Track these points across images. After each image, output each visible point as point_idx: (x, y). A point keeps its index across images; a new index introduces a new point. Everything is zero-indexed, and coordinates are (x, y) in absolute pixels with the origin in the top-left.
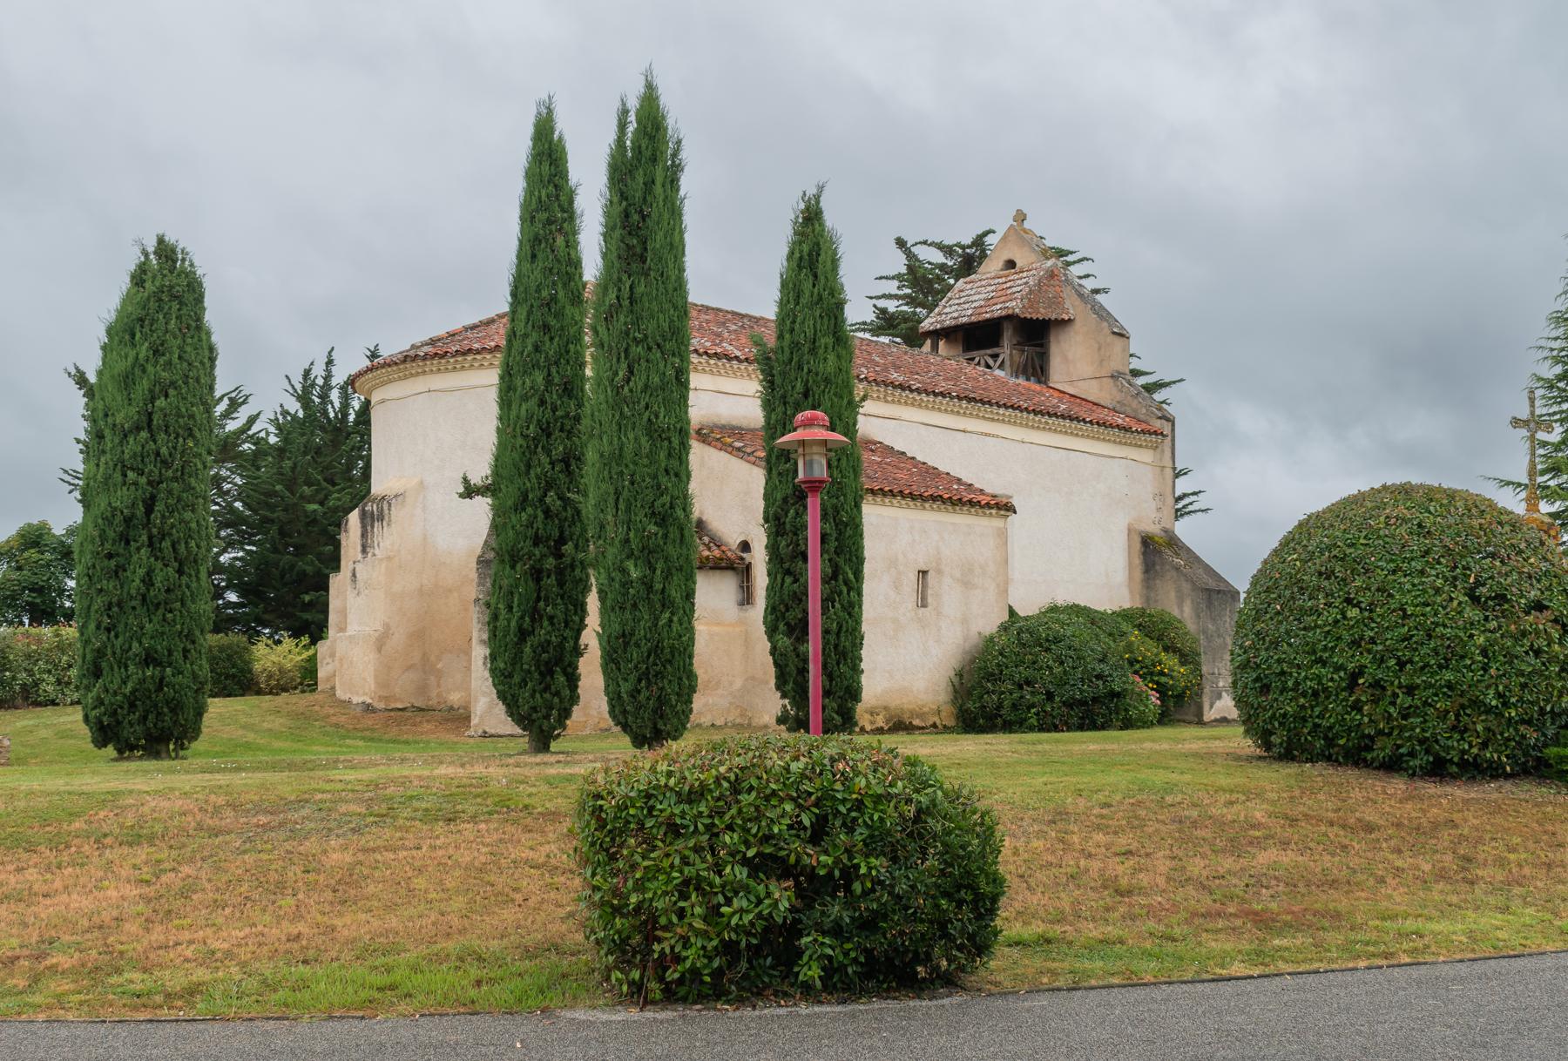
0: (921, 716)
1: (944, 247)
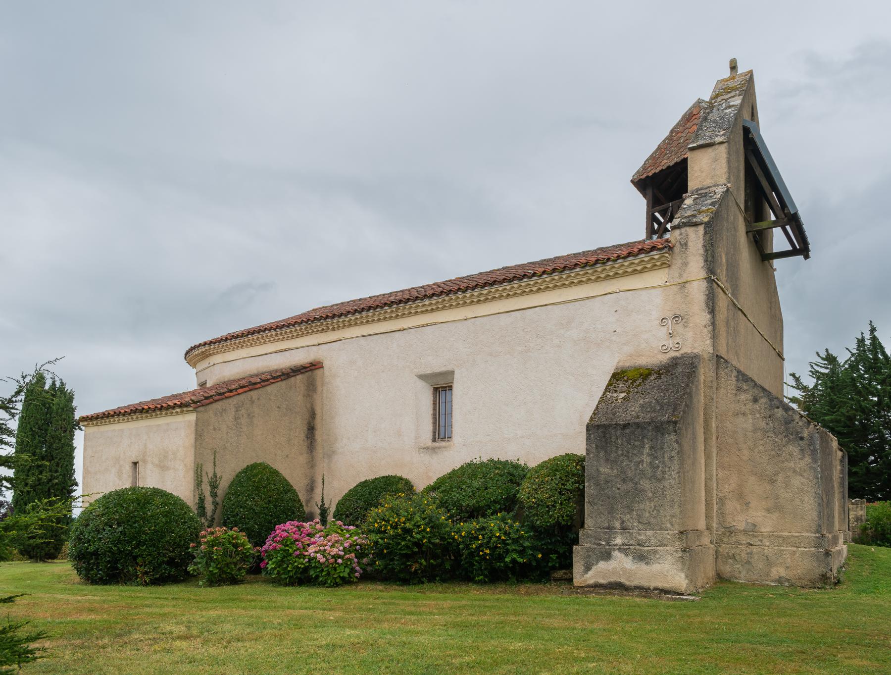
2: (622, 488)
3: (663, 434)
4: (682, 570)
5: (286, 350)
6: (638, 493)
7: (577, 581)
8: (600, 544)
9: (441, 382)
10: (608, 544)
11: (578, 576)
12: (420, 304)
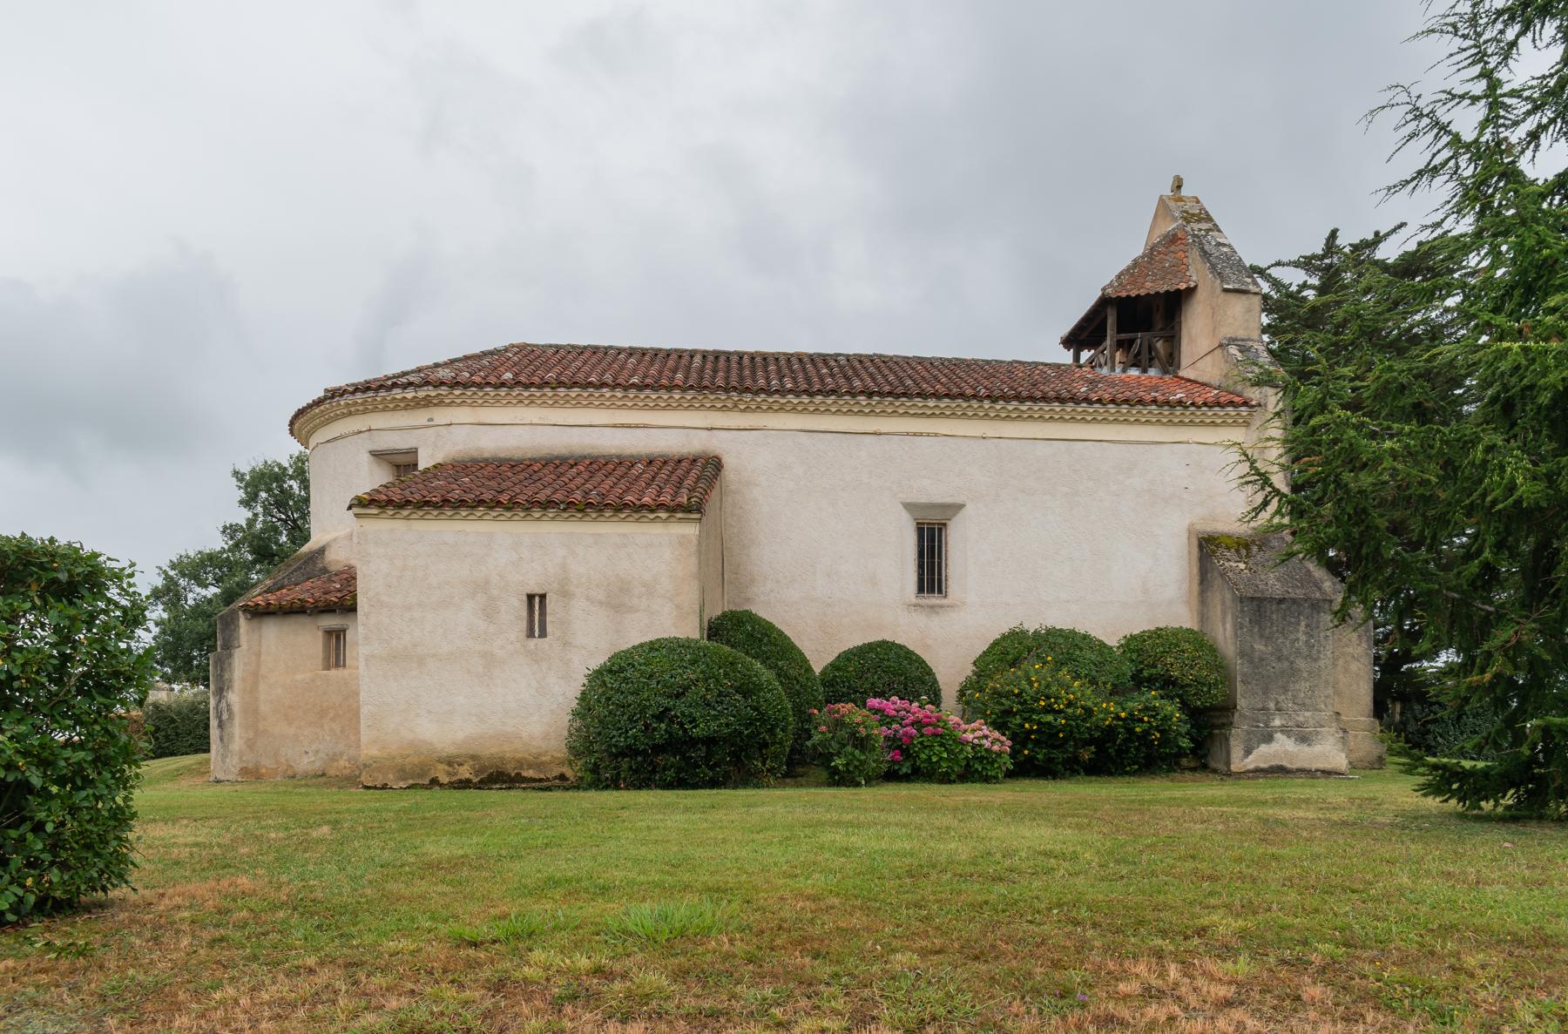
0: (539, 766)
1: (1294, 262)
2: (1277, 667)
3: (1318, 613)
4: (1342, 750)
5: (637, 427)
6: (1294, 673)
7: (1234, 768)
8: (1258, 727)
9: (933, 517)
10: (1267, 726)
11: (1237, 761)
12: (920, 405)
